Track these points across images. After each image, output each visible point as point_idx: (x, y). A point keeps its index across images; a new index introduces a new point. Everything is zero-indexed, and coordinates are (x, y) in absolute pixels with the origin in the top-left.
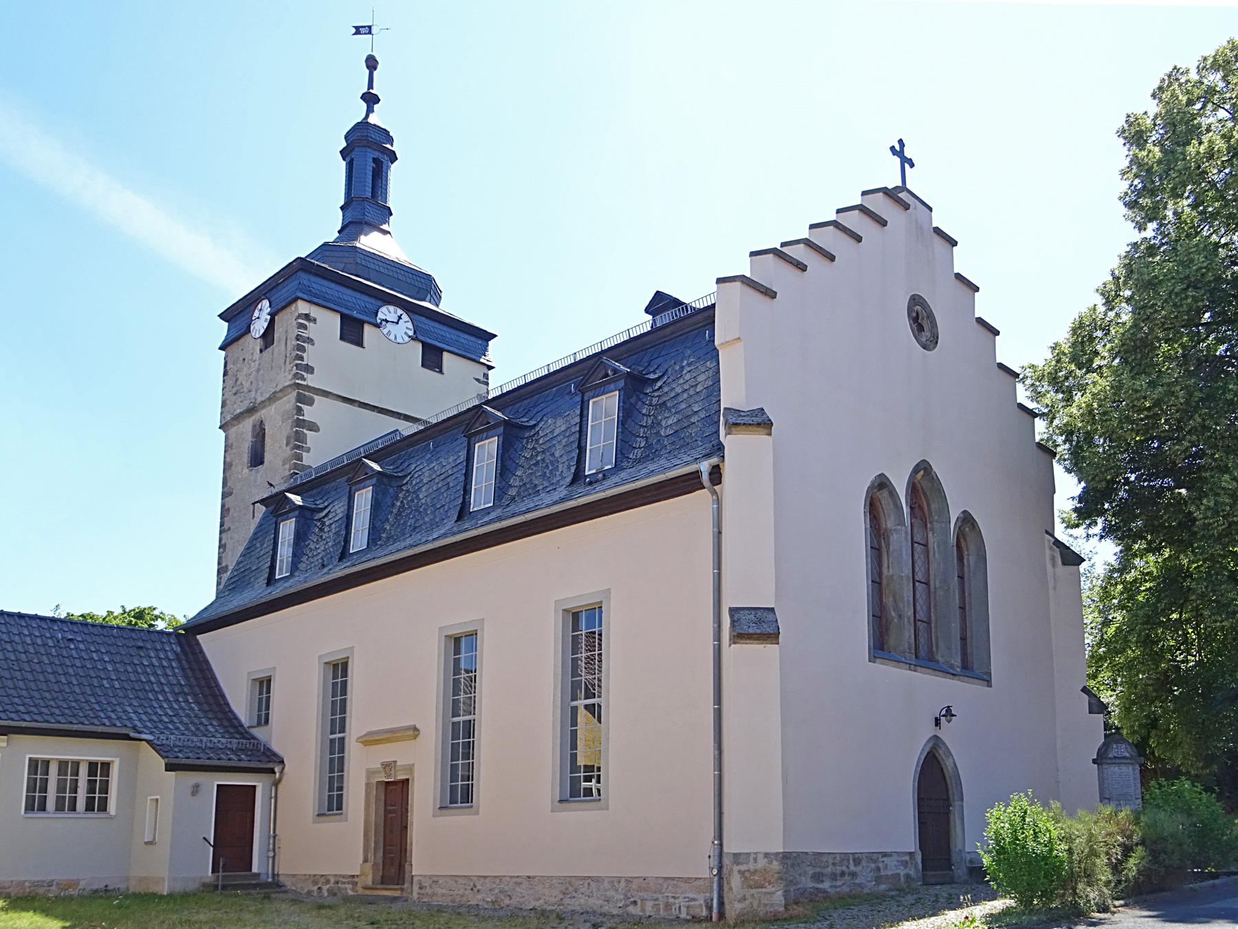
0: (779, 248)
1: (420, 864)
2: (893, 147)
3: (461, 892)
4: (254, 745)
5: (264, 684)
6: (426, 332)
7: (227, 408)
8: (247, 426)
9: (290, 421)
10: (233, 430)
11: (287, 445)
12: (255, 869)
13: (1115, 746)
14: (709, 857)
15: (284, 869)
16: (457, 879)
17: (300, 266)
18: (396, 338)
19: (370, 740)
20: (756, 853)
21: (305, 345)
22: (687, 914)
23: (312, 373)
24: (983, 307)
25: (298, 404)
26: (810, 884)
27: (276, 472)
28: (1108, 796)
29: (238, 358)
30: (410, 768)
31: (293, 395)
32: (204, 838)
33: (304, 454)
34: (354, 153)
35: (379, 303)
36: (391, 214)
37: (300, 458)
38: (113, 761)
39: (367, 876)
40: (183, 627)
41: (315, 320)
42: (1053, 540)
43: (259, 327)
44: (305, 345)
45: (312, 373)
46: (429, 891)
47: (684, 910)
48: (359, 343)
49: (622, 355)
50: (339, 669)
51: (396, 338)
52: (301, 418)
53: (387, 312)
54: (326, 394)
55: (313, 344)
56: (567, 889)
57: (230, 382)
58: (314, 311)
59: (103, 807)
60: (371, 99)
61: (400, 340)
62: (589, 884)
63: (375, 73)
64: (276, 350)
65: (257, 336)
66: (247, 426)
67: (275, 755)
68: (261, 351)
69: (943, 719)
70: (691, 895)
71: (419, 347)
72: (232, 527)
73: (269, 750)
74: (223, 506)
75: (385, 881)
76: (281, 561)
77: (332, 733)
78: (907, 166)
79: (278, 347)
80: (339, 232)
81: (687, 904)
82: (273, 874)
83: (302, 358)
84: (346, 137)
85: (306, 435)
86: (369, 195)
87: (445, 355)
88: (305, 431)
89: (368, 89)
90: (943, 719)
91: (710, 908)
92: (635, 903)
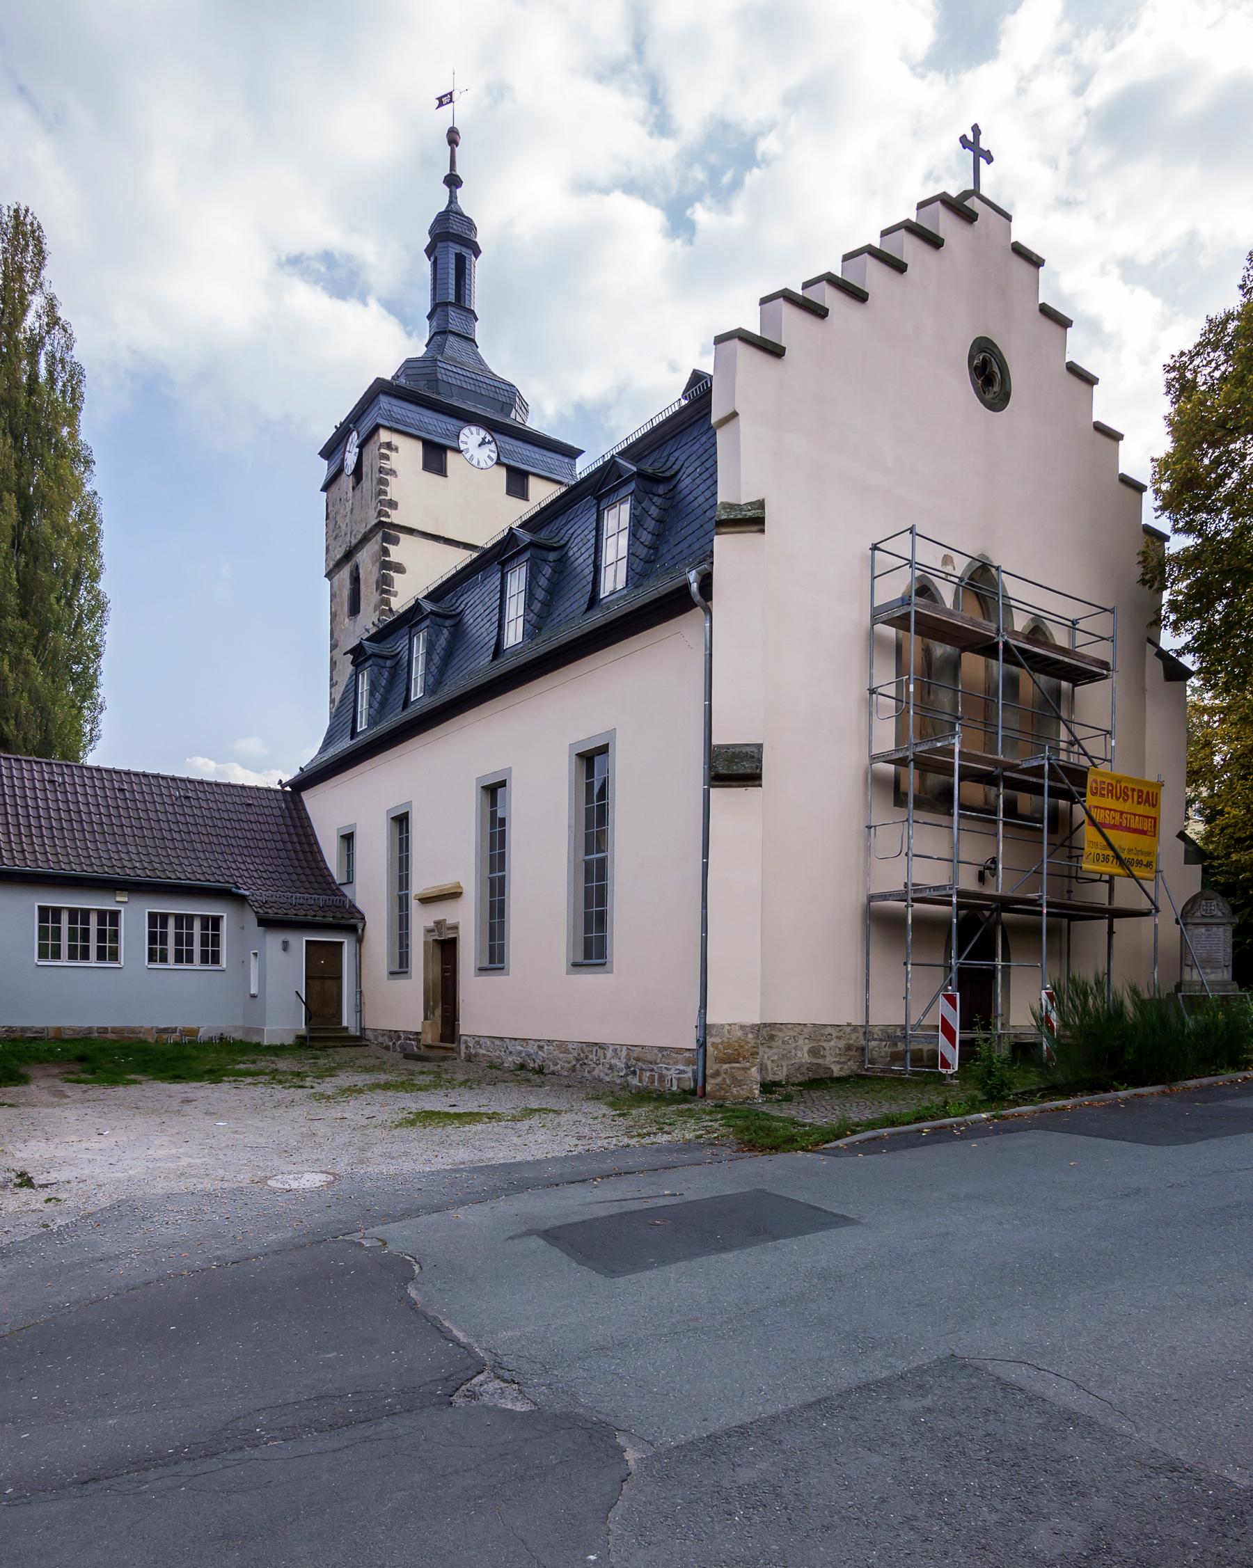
0: (800, 292)
1: (466, 1027)
2: (964, 136)
3: (497, 1054)
4: (333, 901)
5: (348, 839)
6: (510, 454)
7: (329, 555)
8: (345, 573)
9: (378, 564)
10: (336, 578)
11: (377, 589)
12: (345, 1023)
13: (1204, 902)
14: (696, 1027)
15: (369, 1023)
16: (494, 1040)
17: (380, 389)
18: (479, 463)
19: (425, 900)
20: (730, 1025)
21: (388, 477)
22: (678, 1087)
23: (396, 509)
24: (1078, 349)
25: (384, 544)
26: (806, 1058)
27: (368, 620)
28: (1190, 963)
29: (336, 499)
30: (455, 928)
31: (379, 536)
32: (297, 992)
33: (392, 598)
34: (437, 249)
35: (461, 423)
36: (476, 319)
37: (387, 603)
38: (222, 916)
39: (427, 1034)
40: (289, 784)
41: (396, 449)
42: (1156, 650)
43: (351, 459)
44: (388, 477)
45: (396, 509)
46: (473, 1051)
47: (675, 1082)
48: (441, 470)
49: (644, 451)
50: (401, 821)
51: (479, 463)
52: (387, 559)
53: (469, 434)
54: (410, 531)
55: (396, 476)
56: (579, 1055)
57: (331, 526)
58: (396, 440)
59: (216, 960)
60: (453, 181)
61: (483, 465)
62: (597, 1051)
63: (457, 149)
64: (364, 486)
65: (350, 473)
66: (345, 573)
67: (359, 912)
68: (353, 488)
69: (987, 872)
70: (682, 1068)
71: (503, 473)
72: (339, 681)
73: (354, 906)
74: (331, 659)
75: (443, 1038)
76: (361, 712)
77: (400, 891)
78: (982, 161)
79: (366, 483)
80: (427, 346)
81: (678, 1076)
82: (361, 1028)
83: (385, 493)
84: (429, 233)
85: (393, 577)
86: (452, 298)
87: (532, 480)
88: (392, 573)
89: (451, 170)
90: (987, 872)
91: (696, 1081)
92: (634, 1073)
